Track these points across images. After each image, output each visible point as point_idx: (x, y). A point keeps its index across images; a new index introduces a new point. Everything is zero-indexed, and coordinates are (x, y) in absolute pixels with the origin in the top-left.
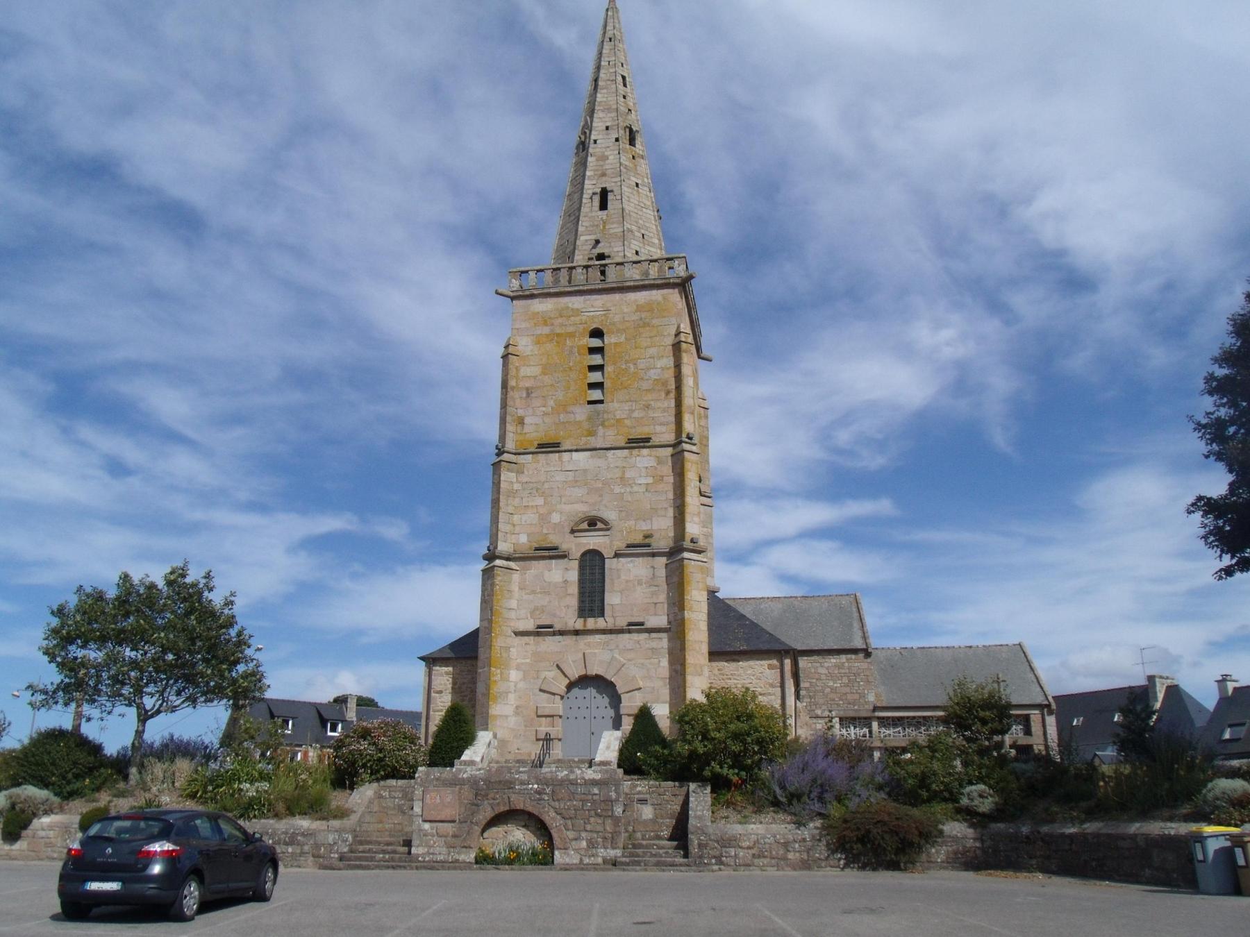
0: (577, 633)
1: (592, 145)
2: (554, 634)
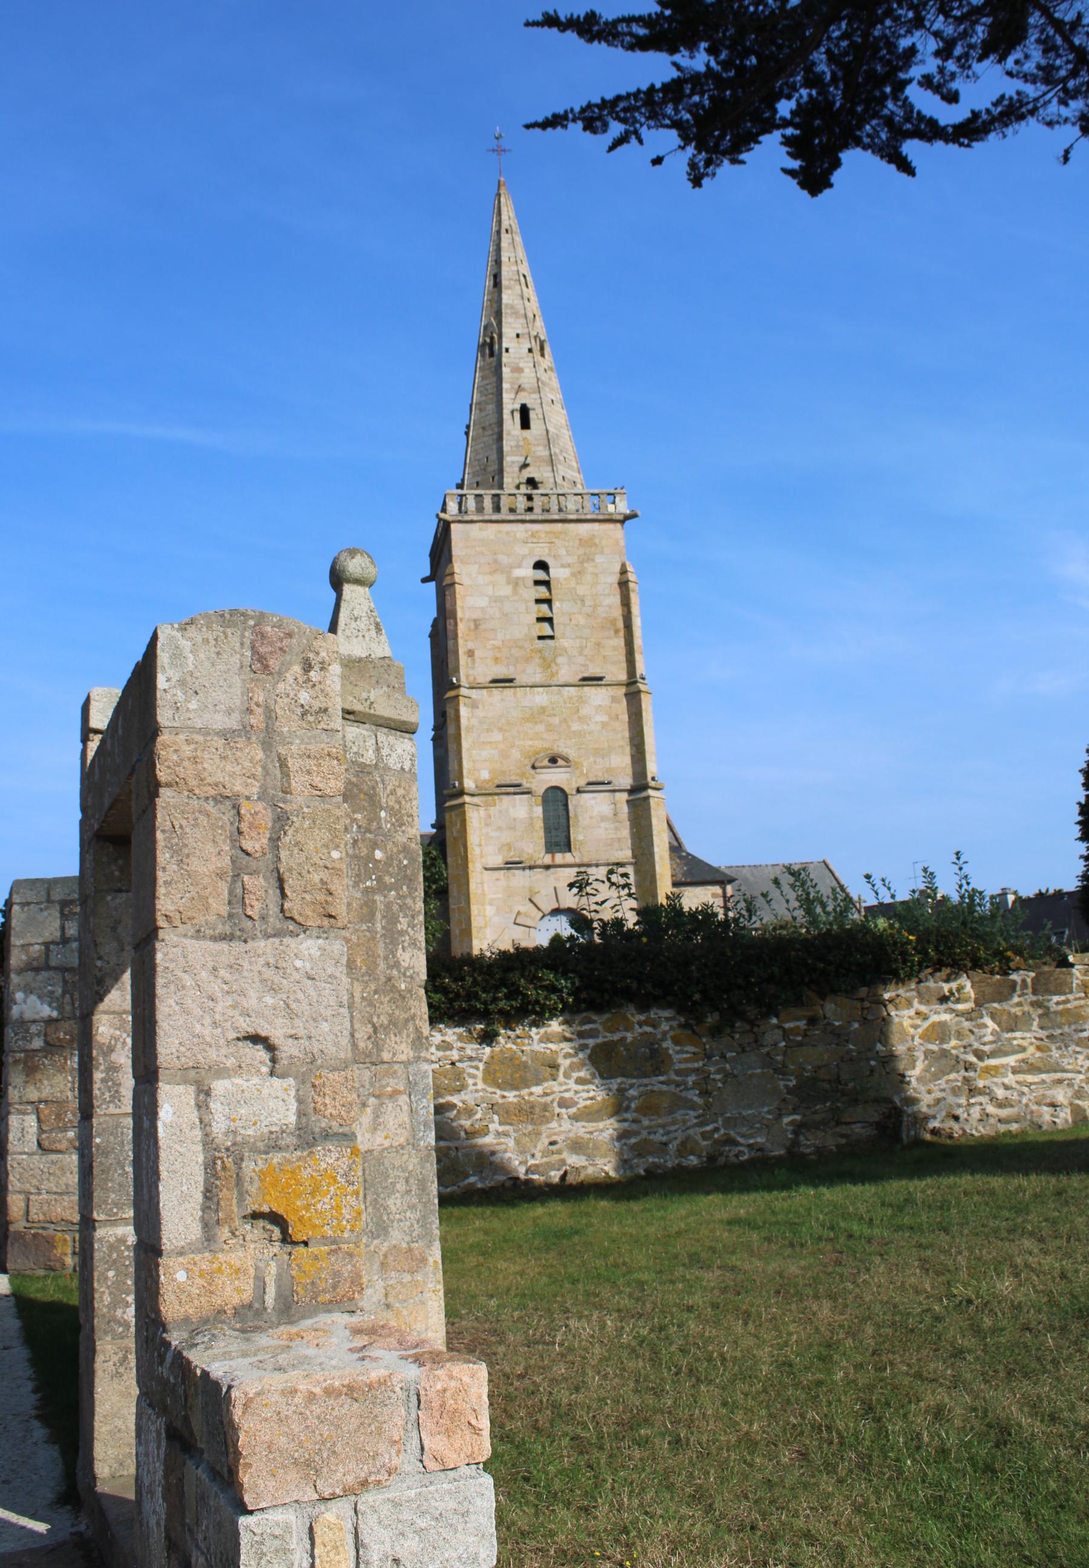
0: (547, 867)
1: (504, 354)
2: (524, 869)
